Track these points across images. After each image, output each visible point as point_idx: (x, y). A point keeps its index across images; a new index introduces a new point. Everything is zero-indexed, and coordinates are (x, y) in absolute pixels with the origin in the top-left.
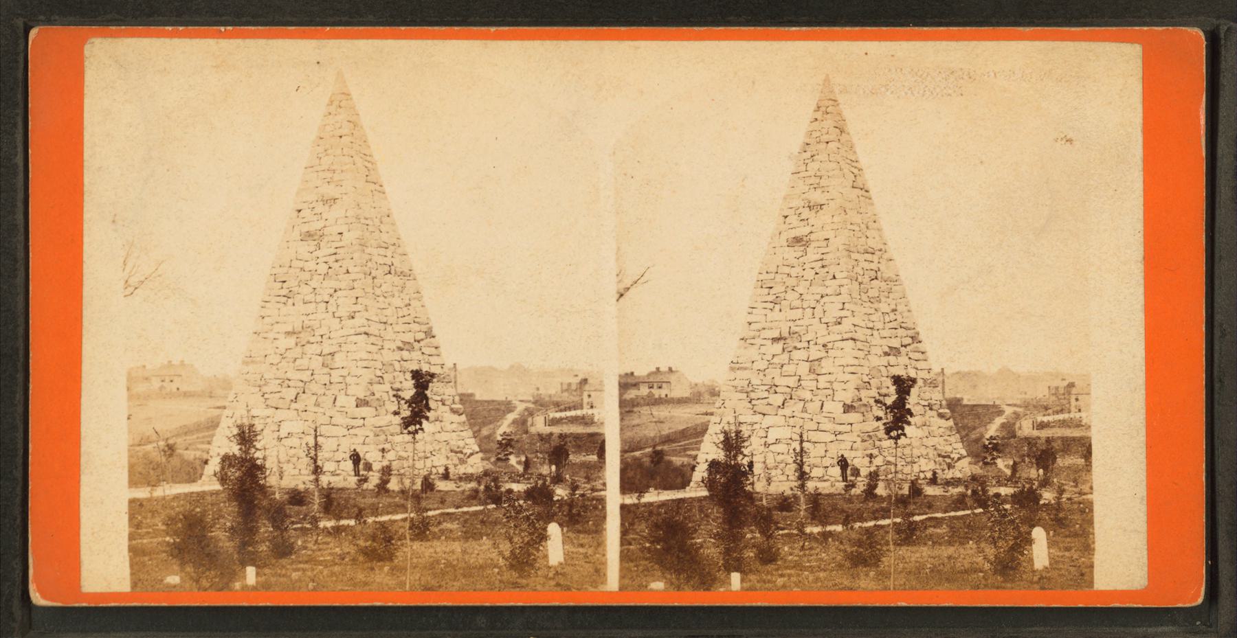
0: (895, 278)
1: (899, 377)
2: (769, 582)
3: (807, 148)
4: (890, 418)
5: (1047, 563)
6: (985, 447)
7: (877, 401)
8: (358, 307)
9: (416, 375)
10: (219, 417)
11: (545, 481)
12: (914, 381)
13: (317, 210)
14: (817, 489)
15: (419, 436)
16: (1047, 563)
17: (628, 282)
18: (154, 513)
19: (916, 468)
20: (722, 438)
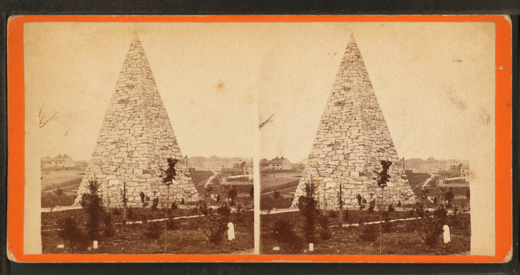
0: (382, 119)
1: (384, 161)
2: (326, 247)
3: (127, 62)
4: (380, 178)
5: (450, 240)
7: (374, 171)
8: (360, 134)
9: (169, 160)
10: (299, 180)
11: (227, 205)
12: (391, 163)
13: (342, 93)
15: (171, 186)
16: (450, 240)
17: (264, 122)
18: (52, 218)
20: (305, 187)
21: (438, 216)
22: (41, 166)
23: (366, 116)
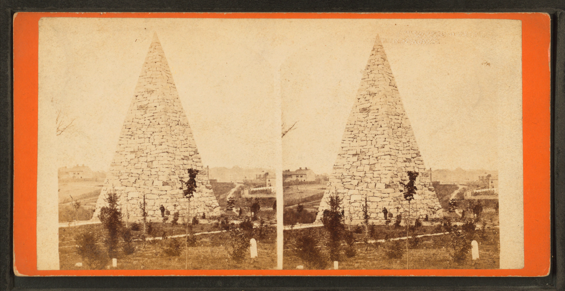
0: (409, 127)
1: (410, 172)
3: (147, 65)
4: (407, 191)
5: (478, 257)
6: (450, 204)
7: (401, 183)
9: (190, 171)
10: (100, 190)
11: (249, 219)
12: (417, 174)
13: (145, 96)
14: (373, 223)
15: (191, 199)
18: (70, 234)
19: (418, 214)
20: (330, 200)
21: (244, 229)
22: (59, 177)
23: (392, 123)
